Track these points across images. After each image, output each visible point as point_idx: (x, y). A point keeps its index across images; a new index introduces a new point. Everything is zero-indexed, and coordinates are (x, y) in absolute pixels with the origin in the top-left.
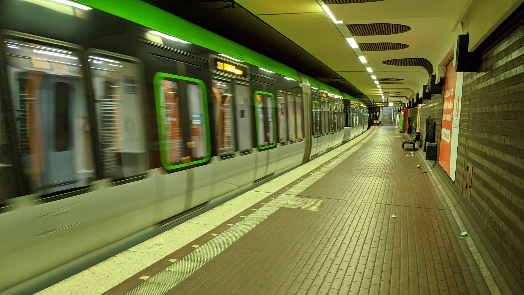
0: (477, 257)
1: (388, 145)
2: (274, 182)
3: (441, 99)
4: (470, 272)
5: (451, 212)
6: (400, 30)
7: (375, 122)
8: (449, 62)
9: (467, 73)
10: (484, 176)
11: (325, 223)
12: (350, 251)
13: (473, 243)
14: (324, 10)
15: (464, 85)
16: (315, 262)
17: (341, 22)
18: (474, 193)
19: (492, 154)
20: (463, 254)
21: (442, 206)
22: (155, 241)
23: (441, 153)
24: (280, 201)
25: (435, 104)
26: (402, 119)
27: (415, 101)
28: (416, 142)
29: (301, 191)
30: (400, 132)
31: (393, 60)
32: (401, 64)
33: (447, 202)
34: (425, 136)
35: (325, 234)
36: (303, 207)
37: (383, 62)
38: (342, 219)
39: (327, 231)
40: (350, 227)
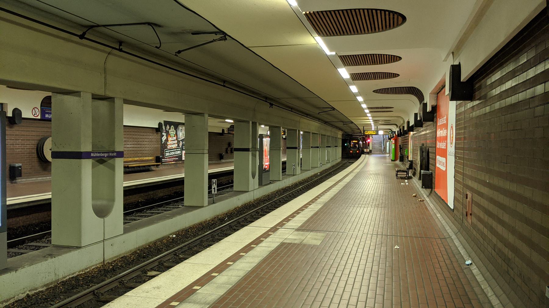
0: (485, 286)
1: (381, 174)
2: (270, 216)
3: (434, 126)
4: (479, 300)
5: (453, 241)
6: (391, 60)
7: (365, 151)
8: (440, 90)
9: (459, 102)
10: (485, 203)
11: (328, 257)
12: (357, 285)
13: (479, 271)
14: (317, 42)
15: (457, 114)
16: (324, 298)
17: (334, 53)
18: (475, 220)
19: (492, 182)
20: (469, 283)
21: (443, 235)
22: (153, 284)
23: (437, 180)
24: (279, 235)
25: (428, 132)
26: (393, 147)
27: (405, 129)
28: (410, 170)
29: (300, 225)
30: (392, 160)
31: (384, 89)
32: (391, 93)
33: (448, 231)
34: (419, 164)
35: (330, 269)
36: (304, 242)
37: (374, 91)
38: (345, 253)
39: (331, 265)
40: (354, 260)
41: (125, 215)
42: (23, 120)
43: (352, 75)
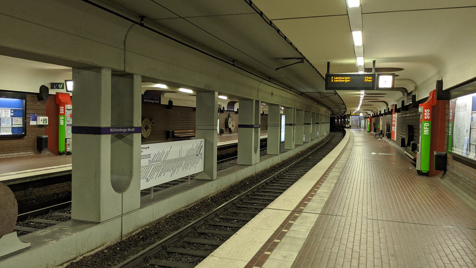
7: (346, 126)
26: (369, 124)
27: (378, 114)
30: (368, 132)
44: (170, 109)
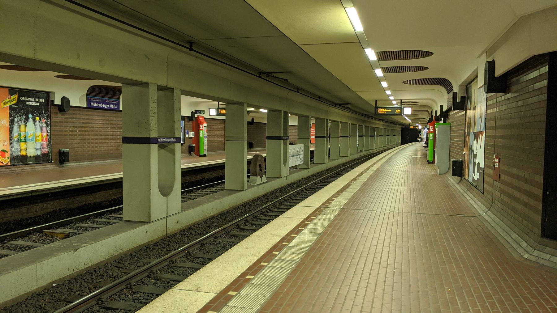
41: (183, 193)
42: (71, 108)
43: (379, 54)
44: (253, 125)
